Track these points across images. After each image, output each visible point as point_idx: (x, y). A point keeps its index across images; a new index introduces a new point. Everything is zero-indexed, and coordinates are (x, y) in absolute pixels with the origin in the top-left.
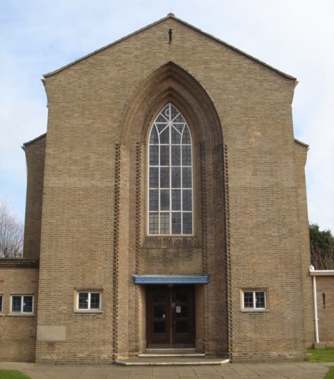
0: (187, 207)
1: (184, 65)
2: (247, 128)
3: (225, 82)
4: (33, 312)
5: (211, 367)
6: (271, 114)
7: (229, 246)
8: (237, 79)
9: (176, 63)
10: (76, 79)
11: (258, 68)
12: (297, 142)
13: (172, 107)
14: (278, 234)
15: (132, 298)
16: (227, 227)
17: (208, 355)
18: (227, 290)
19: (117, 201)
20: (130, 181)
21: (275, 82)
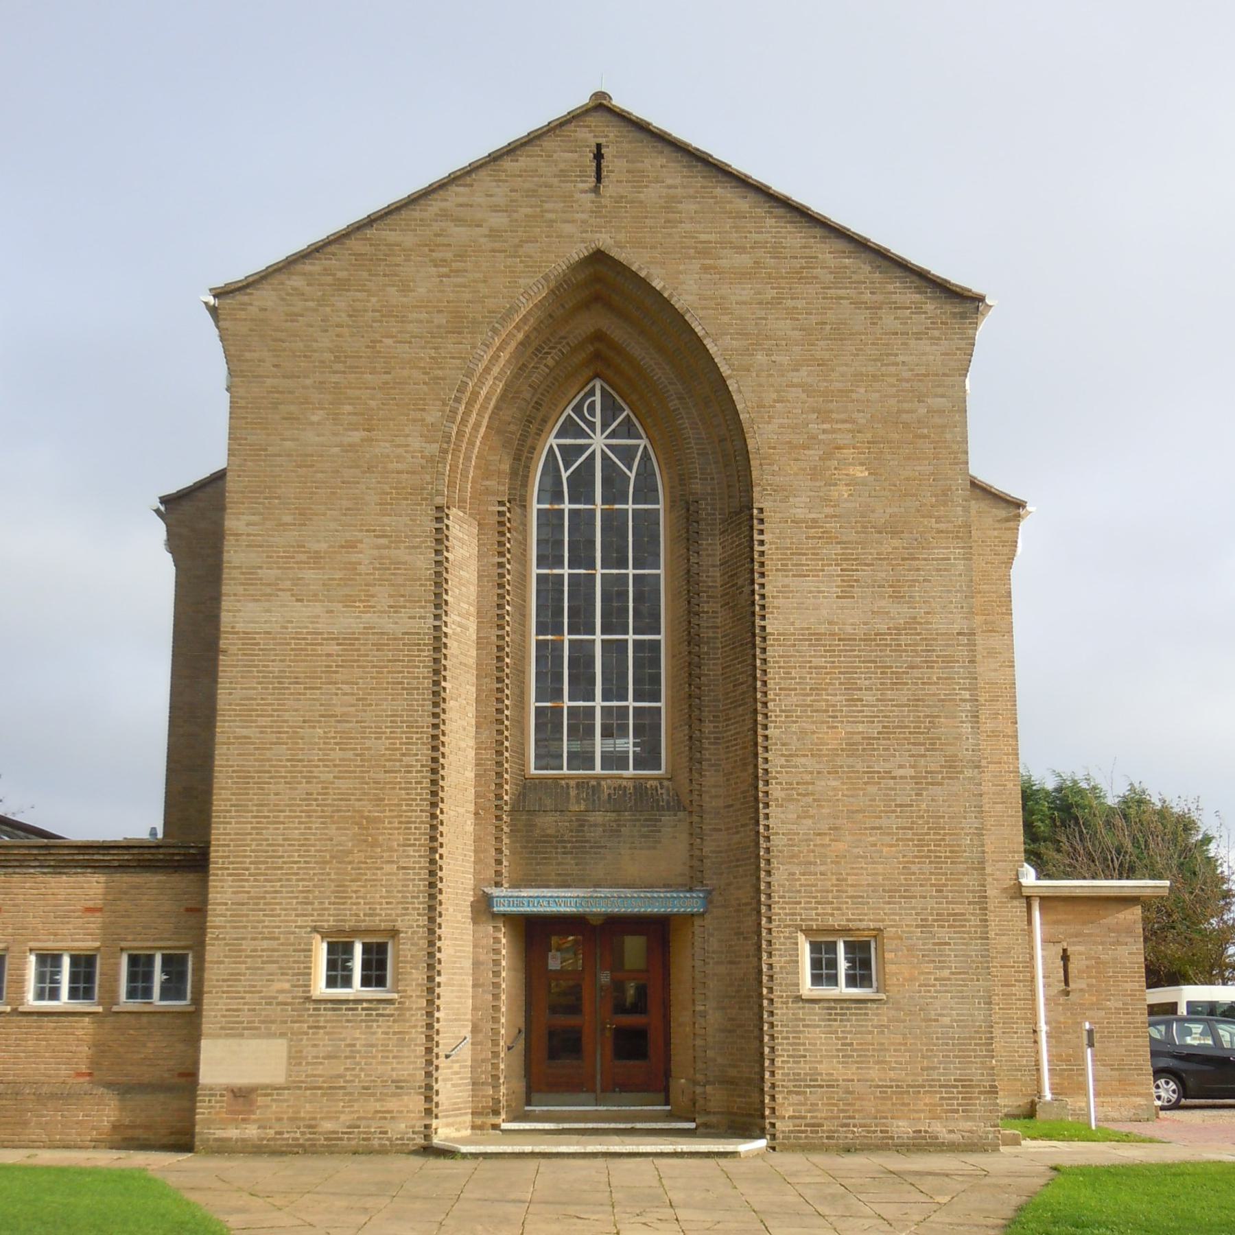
0: (647, 690)
1: (637, 260)
2: (827, 456)
3: (762, 314)
4: (187, 1002)
5: (710, 1162)
6: (899, 412)
7: (767, 805)
8: (800, 304)
9: (615, 253)
10: (311, 304)
11: (868, 268)
12: (980, 490)
13: (602, 388)
14: (912, 772)
15: (482, 958)
16: (760, 750)
17: (706, 1125)
18: (759, 935)
19: (438, 671)
20: (479, 614)
21: (919, 310)
